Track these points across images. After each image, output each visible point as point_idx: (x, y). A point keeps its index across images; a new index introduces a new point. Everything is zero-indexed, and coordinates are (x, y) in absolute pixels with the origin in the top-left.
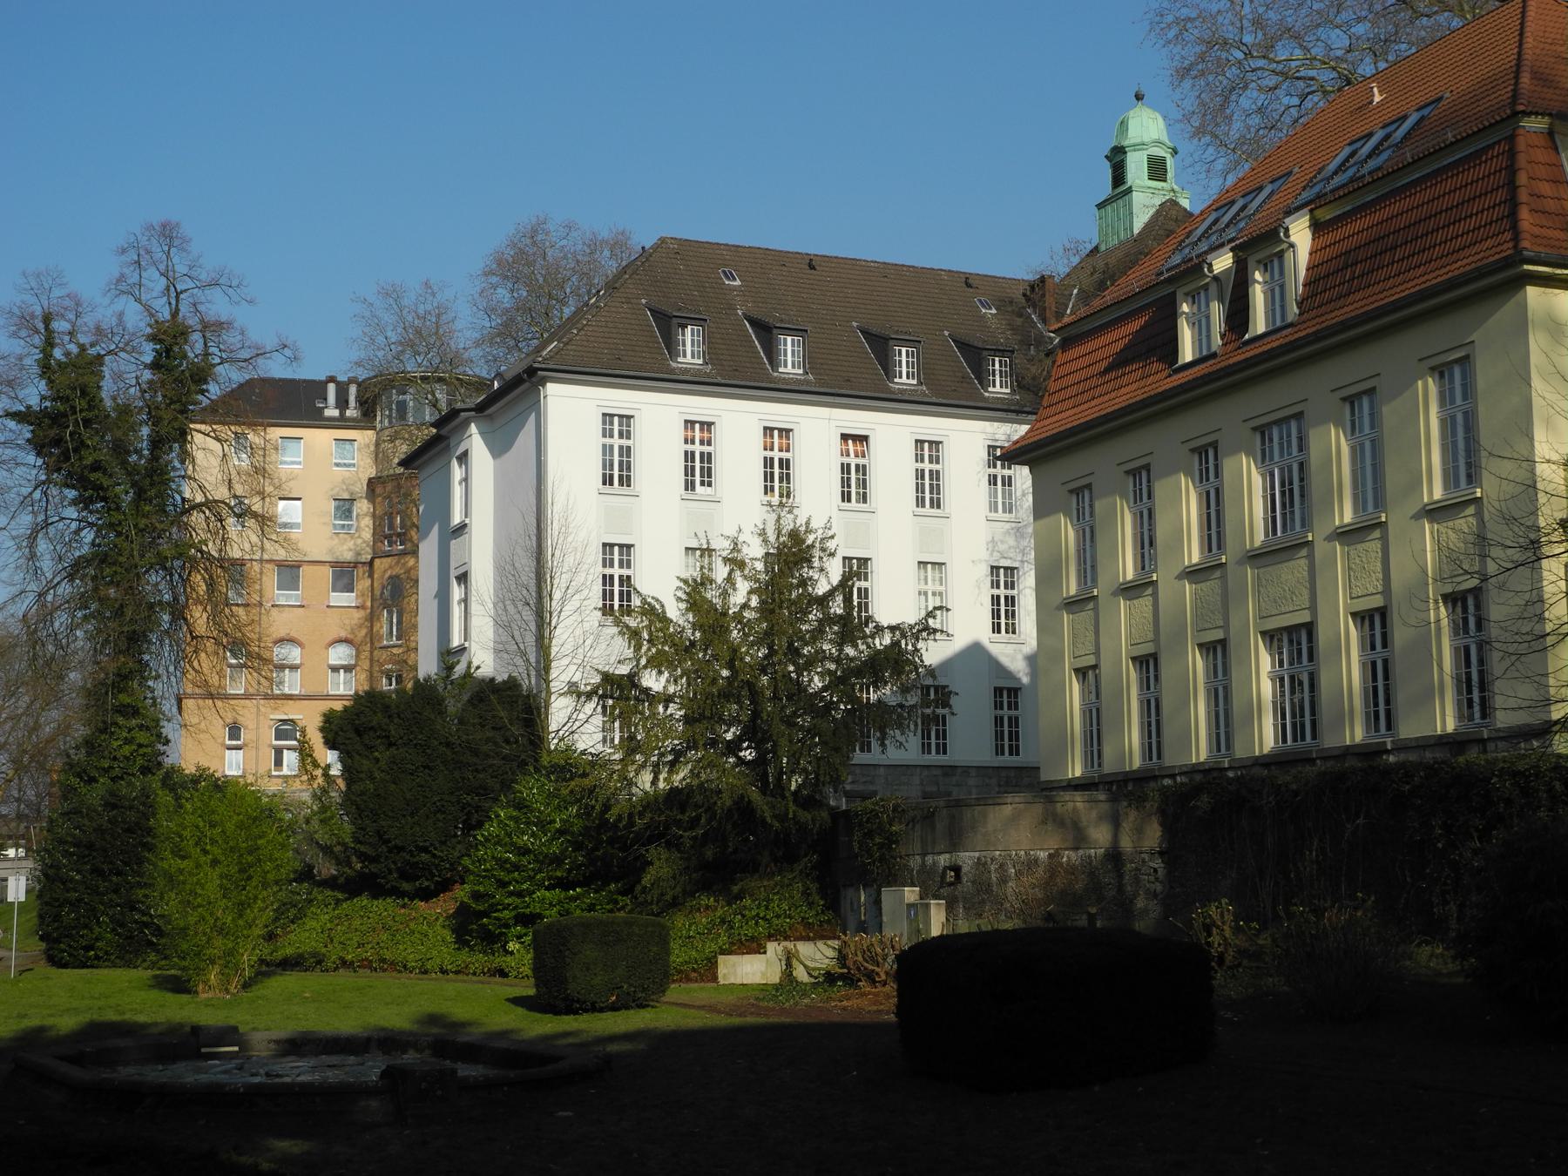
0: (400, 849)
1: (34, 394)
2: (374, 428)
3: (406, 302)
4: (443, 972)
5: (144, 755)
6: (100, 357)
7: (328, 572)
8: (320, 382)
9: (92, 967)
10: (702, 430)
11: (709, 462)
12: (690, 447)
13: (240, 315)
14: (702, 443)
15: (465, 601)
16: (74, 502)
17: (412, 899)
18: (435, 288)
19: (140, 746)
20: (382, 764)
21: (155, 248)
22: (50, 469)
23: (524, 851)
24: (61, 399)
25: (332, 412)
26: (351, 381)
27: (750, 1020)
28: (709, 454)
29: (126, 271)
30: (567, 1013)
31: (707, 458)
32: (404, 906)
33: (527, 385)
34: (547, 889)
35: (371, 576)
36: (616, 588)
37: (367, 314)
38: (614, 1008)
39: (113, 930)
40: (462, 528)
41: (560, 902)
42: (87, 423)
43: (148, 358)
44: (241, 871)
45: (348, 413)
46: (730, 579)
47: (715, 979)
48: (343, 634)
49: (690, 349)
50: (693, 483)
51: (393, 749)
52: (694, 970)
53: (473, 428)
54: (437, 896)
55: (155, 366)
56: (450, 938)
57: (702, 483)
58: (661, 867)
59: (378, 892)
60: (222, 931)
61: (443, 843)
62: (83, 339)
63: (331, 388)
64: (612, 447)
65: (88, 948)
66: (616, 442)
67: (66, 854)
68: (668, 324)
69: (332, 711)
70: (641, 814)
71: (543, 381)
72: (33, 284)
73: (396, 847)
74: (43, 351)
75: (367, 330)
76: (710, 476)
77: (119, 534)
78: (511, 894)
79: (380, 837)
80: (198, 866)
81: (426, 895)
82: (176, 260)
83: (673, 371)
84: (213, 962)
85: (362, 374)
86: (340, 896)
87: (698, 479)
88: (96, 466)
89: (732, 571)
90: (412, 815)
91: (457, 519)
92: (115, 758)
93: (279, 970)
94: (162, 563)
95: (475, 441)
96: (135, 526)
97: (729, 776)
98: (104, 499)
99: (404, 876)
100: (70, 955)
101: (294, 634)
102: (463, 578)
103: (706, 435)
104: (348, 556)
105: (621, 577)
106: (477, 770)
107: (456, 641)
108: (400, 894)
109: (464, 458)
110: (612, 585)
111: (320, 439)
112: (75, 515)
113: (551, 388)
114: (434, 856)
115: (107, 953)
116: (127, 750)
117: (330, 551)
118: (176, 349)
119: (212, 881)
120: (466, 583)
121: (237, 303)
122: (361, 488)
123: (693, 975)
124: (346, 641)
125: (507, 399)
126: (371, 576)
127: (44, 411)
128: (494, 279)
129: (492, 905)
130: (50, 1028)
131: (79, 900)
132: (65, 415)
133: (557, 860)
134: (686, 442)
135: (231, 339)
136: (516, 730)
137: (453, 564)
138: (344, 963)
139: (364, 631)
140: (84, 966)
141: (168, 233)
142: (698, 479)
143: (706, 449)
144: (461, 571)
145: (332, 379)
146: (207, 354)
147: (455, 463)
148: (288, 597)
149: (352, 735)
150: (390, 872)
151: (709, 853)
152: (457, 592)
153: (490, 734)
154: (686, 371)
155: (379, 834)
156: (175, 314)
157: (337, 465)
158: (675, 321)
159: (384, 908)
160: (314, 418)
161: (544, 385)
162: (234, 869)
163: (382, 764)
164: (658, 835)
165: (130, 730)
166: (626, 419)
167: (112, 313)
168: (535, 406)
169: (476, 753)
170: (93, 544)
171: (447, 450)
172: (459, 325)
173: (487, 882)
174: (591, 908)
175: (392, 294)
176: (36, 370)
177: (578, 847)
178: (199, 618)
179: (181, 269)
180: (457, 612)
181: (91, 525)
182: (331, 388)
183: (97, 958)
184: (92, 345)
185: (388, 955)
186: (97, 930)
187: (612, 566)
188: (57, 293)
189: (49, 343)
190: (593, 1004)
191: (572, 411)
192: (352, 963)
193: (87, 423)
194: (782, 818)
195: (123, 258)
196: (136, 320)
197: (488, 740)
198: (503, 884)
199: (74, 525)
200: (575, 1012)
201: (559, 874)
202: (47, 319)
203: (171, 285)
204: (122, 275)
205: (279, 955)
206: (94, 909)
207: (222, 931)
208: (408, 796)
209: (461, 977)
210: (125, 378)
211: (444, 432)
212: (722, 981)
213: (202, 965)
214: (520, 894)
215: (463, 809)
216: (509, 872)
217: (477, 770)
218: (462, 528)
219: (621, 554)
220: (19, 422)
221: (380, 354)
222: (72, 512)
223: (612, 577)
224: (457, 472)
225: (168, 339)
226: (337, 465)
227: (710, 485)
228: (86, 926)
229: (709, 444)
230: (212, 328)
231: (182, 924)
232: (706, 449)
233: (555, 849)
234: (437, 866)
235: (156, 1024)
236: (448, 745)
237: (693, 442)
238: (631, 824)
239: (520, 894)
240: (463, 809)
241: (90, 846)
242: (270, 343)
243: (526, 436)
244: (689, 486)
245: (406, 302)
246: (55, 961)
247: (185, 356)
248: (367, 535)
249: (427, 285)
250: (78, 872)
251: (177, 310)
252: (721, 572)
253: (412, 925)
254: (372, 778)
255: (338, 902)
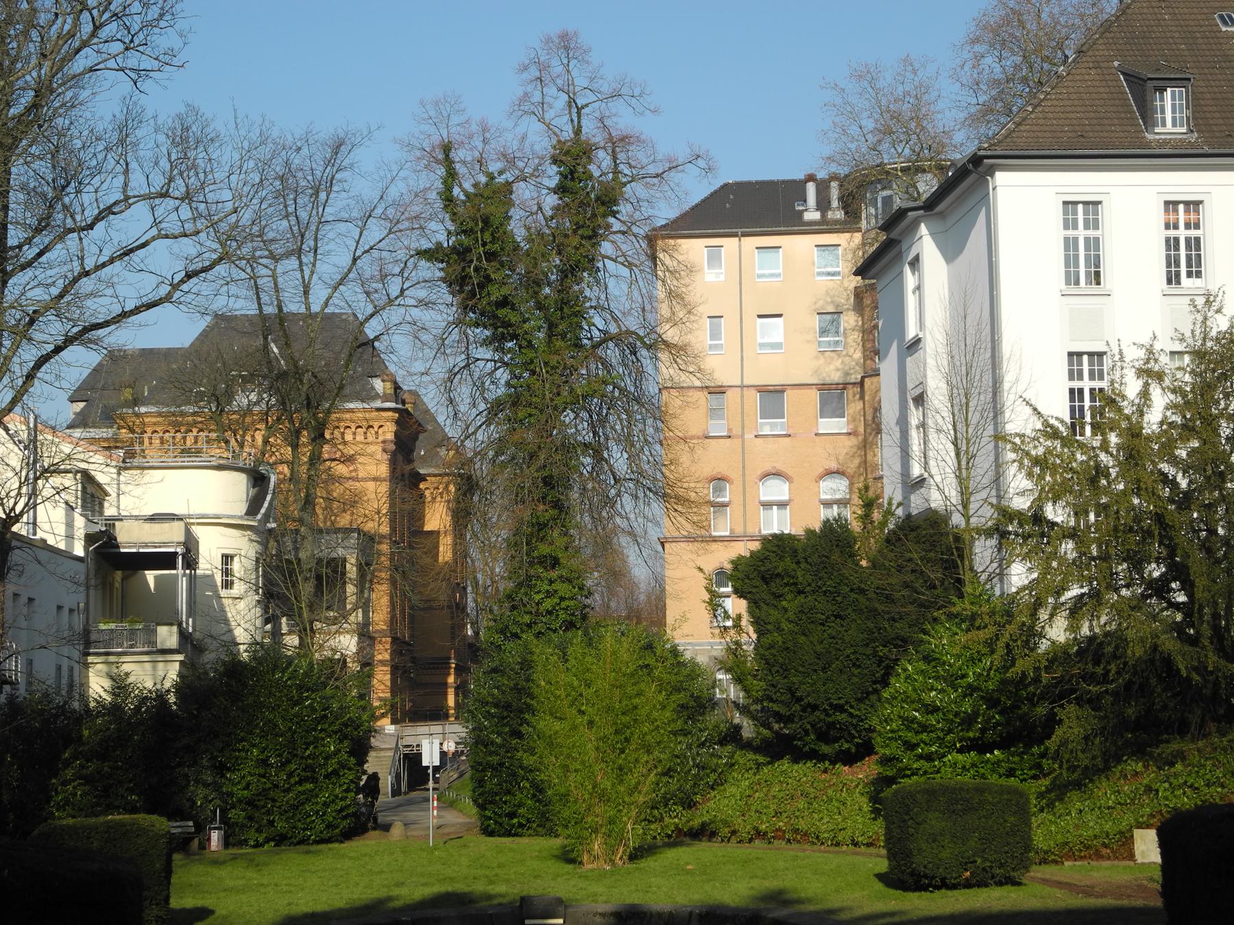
0: (814, 707)
1: (440, 232)
2: (859, 230)
3: (881, 84)
4: (856, 844)
5: (566, 609)
6: (509, 184)
7: (814, 395)
8: (801, 181)
9: (516, 835)
10: (1187, 211)
11: (1198, 248)
12: (1172, 233)
13: (643, 126)
14: (1188, 226)
15: (923, 425)
16: (486, 343)
17: (833, 763)
18: (917, 65)
19: (562, 599)
20: (790, 614)
21: (555, 62)
22: (465, 308)
23: (932, 709)
24: (464, 232)
25: (812, 215)
26: (834, 177)
27: (1125, 902)
28: (1197, 240)
29: (529, 88)
30: (914, 890)
31: (1195, 244)
32: (825, 771)
33: (973, 177)
34: (960, 751)
35: (862, 398)
36: (1087, 403)
37: (839, 101)
38: (968, 885)
39: (534, 796)
40: (916, 343)
41: (974, 765)
42: (491, 256)
43: (553, 182)
44: (617, 732)
45: (830, 215)
46: (1145, 394)
47: (1131, 856)
48: (834, 465)
49: (1171, 115)
50: (1178, 274)
51: (801, 598)
52: (1105, 846)
53: (923, 229)
54: (862, 758)
55: (561, 190)
56: (866, 807)
57: (1189, 275)
58: (1073, 725)
59: (799, 756)
60: (603, 797)
61: (860, 700)
62: (494, 167)
63: (811, 189)
64: (1076, 239)
65: (512, 815)
66: (1081, 233)
67: (489, 716)
68: (1143, 89)
69: (740, 558)
70: (1048, 669)
71: (991, 171)
72: (432, 113)
73: (809, 705)
74: (445, 182)
75: (837, 120)
76: (1199, 264)
77: (533, 373)
78: (920, 757)
79: (793, 695)
80: (574, 727)
81: (850, 759)
82: (575, 73)
83: (1148, 145)
84: (596, 831)
85: (843, 171)
86: (761, 759)
87: (1183, 269)
88: (504, 302)
89: (1146, 385)
90: (824, 669)
91: (911, 332)
92: (538, 614)
93: (687, 840)
94: (578, 402)
95: (926, 244)
96: (546, 364)
97: (1155, 627)
98: (514, 337)
99: (823, 737)
100: (496, 822)
101: (780, 467)
102: (920, 400)
103: (1192, 216)
104: (836, 377)
105: (1092, 390)
106: (894, 619)
107: (916, 470)
108: (821, 758)
109: (915, 263)
110: (1081, 399)
111: (800, 246)
112: (488, 356)
113: (1002, 179)
114: (851, 715)
115: (528, 820)
116: (548, 604)
117: (816, 372)
118: (580, 169)
119: (588, 741)
120: (923, 405)
121: (642, 114)
122: (847, 300)
123: (1105, 851)
124: (840, 473)
125: (959, 189)
126: (862, 398)
127: (454, 249)
128: (978, 48)
129: (901, 770)
130: (390, 899)
131: (501, 764)
132: (468, 250)
133: (969, 721)
134: (1167, 227)
135: (639, 155)
136: (936, 575)
137: (910, 385)
138: (759, 834)
139: (857, 461)
140: (509, 834)
141: (566, 44)
142: (1183, 269)
143: (1193, 233)
144: (918, 391)
145: (811, 178)
146: (616, 172)
147: (907, 269)
148: (773, 426)
149: (758, 582)
150: (807, 733)
151: (1131, 712)
152: (915, 417)
153: (909, 578)
154: (1165, 143)
155: (791, 691)
156: (578, 131)
157: (819, 274)
158: (1150, 84)
159: (801, 773)
160: (792, 223)
161: (992, 175)
162: (609, 731)
163: (790, 614)
164: (1061, 693)
165: (551, 582)
166: (1093, 205)
167: (513, 134)
168: (982, 198)
169: (889, 599)
170: (508, 384)
171: (899, 256)
172: (941, 105)
173: (894, 744)
174: (1011, 773)
175: (866, 75)
176: (439, 205)
177: (992, 702)
178: (619, 459)
179: (581, 82)
180: (915, 438)
181: (506, 364)
182: (811, 189)
183: (521, 825)
184: (501, 173)
185: (802, 825)
186: (519, 796)
187: (1081, 378)
188: (455, 120)
189: (451, 176)
190: (943, 880)
191: (1026, 201)
192: (765, 834)
193: (491, 256)
194: (1201, 669)
195: (525, 75)
196: (540, 143)
197: (906, 585)
198: (910, 747)
199: (490, 365)
200: (924, 888)
201: (971, 734)
202: (447, 148)
203: (572, 102)
204: (526, 94)
205: (696, 823)
206: (514, 775)
207: (603, 797)
208: (819, 648)
209: (872, 850)
210: (534, 204)
211: (894, 234)
212: (1139, 859)
213: (586, 833)
214: (929, 758)
215: (881, 661)
216: (917, 733)
217: (894, 619)
218: (916, 343)
219: (1091, 363)
220: (429, 260)
221: (853, 146)
222: (484, 353)
223: (1081, 391)
224: (910, 280)
225: (572, 160)
226: (819, 274)
227: (1199, 274)
228: (509, 792)
229: (1197, 226)
230: (618, 143)
231: (563, 790)
232: (1193, 233)
233: (967, 707)
234: (855, 726)
235: (490, 897)
236: (862, 591)
237: (1176, 227)
238: (1037, 680)
239: (929, 758)
240: (881, 661)
241: (508, 706)
242: (682, 154)
243: (977, 235)
244: (1173, 279)
245: (881, 84)
246: (488, 832)
247: (591, 177)
248: (858, 355)
249: (907, 61)
250: (499, 734)
251: (580, 127)
252: (1132, 388)
253: (830, 792)
254: (779, 629)
255: (759, 766)
